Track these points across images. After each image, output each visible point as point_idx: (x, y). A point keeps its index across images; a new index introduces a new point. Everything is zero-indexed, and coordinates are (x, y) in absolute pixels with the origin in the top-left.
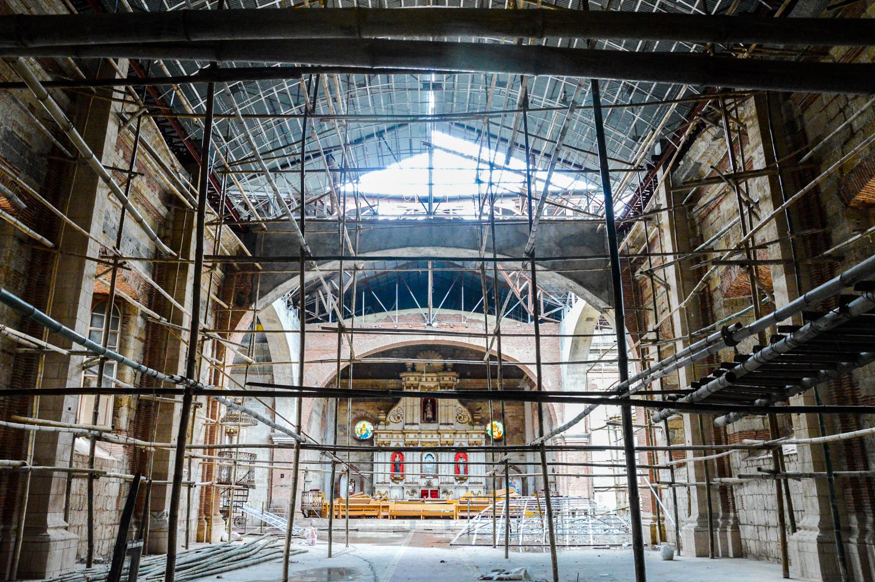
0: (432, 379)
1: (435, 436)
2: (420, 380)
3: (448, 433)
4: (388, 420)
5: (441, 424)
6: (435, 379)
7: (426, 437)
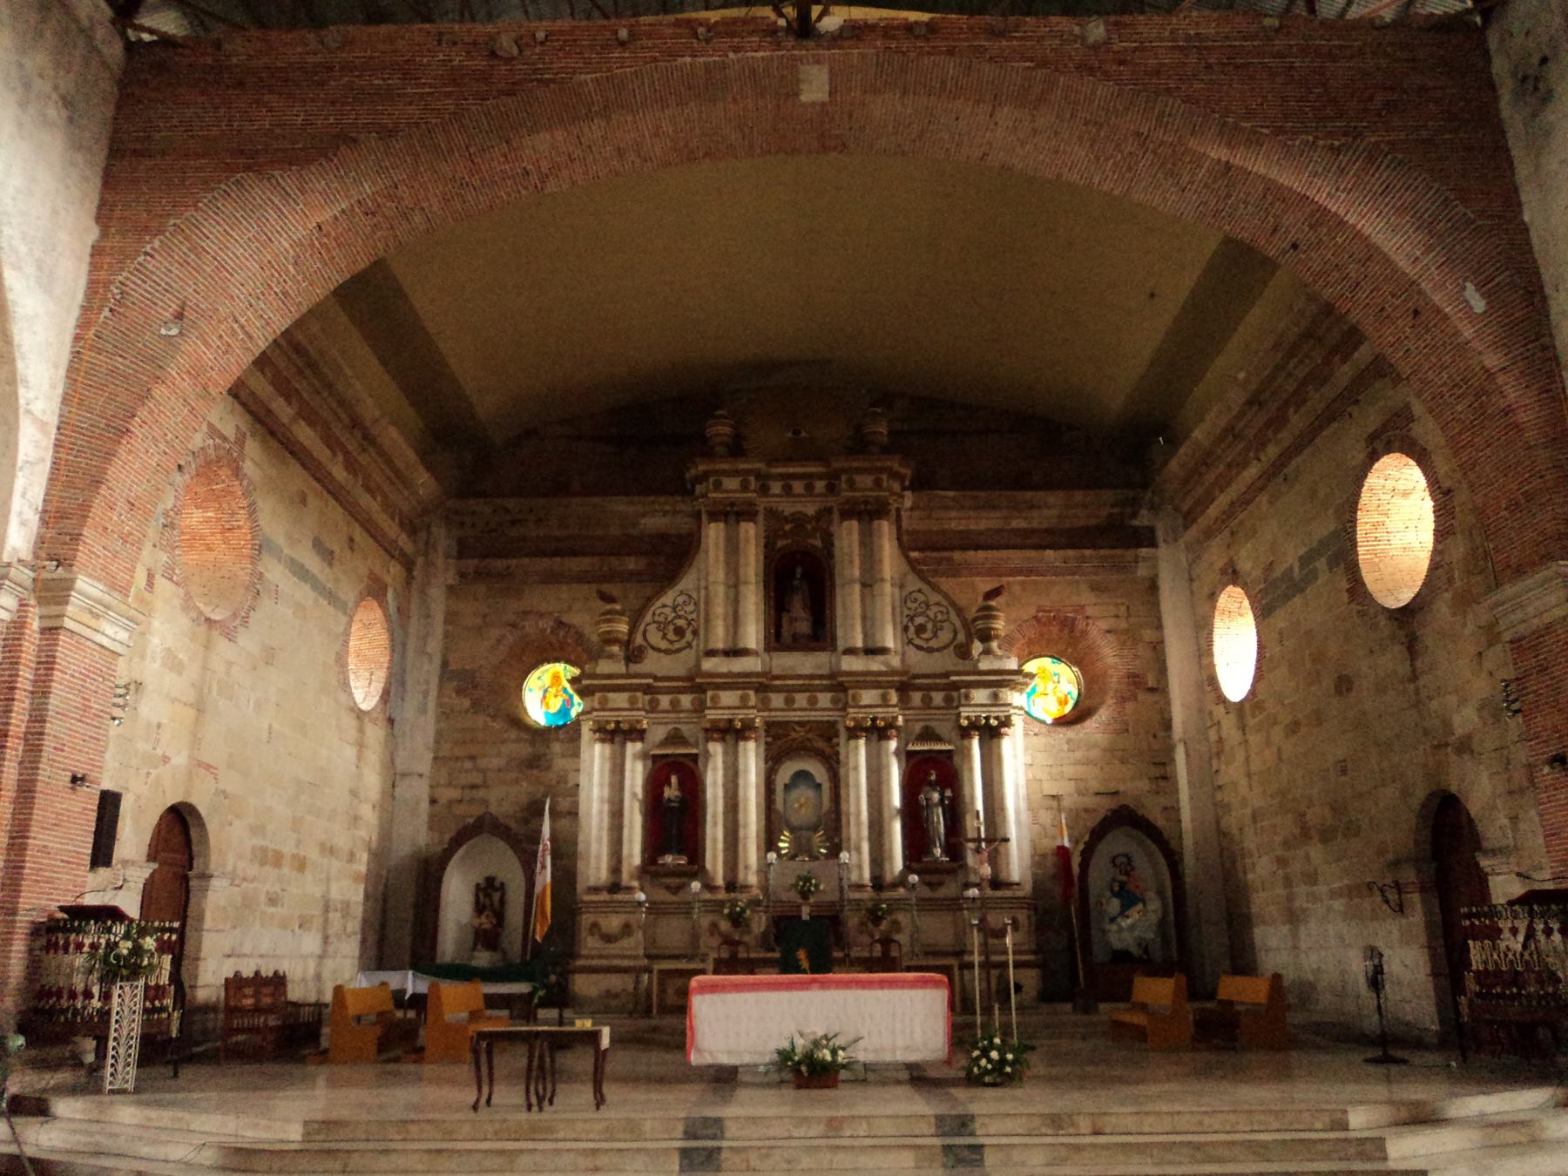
0: (809, 488)
1: (824, 699)
2: (764, 490)
3: (877, 685)
4: (639, 640)
5: (850, 651)
6: (820, 486)
7: (789, 702)
